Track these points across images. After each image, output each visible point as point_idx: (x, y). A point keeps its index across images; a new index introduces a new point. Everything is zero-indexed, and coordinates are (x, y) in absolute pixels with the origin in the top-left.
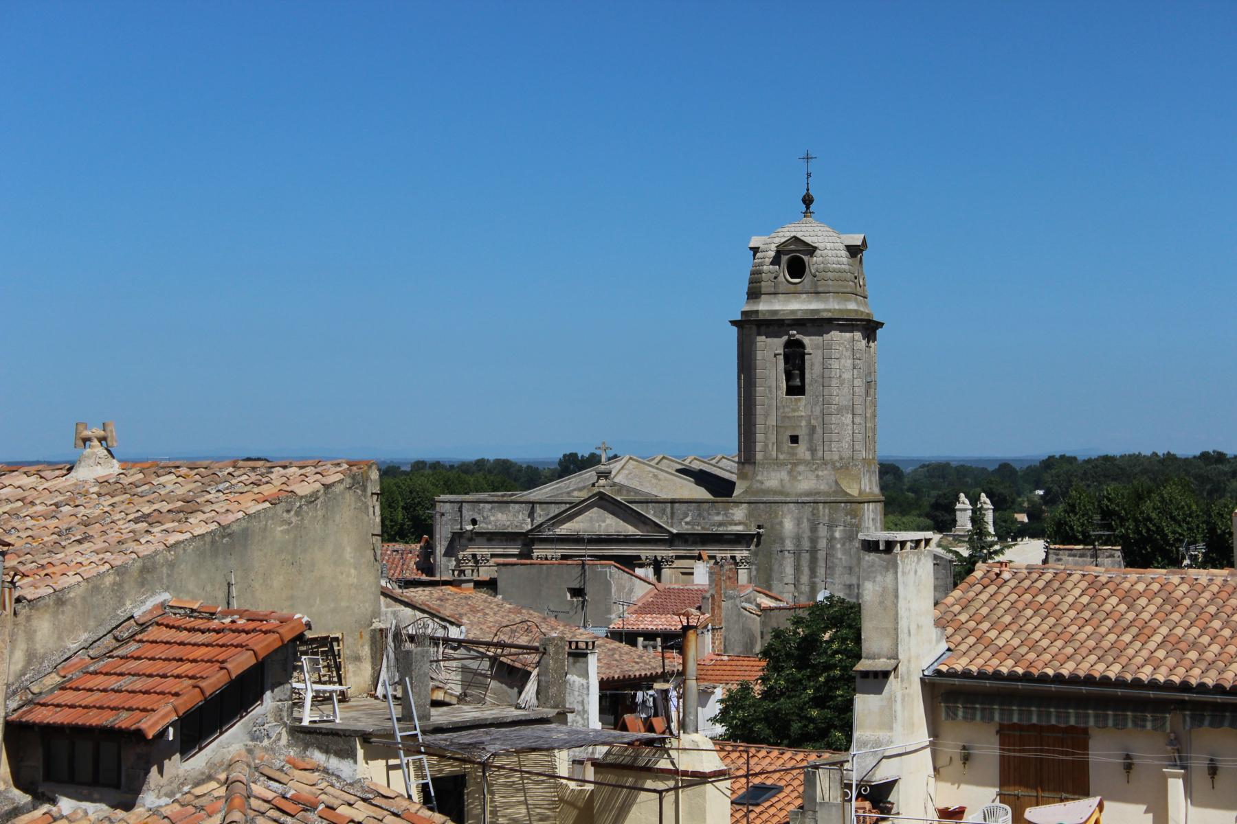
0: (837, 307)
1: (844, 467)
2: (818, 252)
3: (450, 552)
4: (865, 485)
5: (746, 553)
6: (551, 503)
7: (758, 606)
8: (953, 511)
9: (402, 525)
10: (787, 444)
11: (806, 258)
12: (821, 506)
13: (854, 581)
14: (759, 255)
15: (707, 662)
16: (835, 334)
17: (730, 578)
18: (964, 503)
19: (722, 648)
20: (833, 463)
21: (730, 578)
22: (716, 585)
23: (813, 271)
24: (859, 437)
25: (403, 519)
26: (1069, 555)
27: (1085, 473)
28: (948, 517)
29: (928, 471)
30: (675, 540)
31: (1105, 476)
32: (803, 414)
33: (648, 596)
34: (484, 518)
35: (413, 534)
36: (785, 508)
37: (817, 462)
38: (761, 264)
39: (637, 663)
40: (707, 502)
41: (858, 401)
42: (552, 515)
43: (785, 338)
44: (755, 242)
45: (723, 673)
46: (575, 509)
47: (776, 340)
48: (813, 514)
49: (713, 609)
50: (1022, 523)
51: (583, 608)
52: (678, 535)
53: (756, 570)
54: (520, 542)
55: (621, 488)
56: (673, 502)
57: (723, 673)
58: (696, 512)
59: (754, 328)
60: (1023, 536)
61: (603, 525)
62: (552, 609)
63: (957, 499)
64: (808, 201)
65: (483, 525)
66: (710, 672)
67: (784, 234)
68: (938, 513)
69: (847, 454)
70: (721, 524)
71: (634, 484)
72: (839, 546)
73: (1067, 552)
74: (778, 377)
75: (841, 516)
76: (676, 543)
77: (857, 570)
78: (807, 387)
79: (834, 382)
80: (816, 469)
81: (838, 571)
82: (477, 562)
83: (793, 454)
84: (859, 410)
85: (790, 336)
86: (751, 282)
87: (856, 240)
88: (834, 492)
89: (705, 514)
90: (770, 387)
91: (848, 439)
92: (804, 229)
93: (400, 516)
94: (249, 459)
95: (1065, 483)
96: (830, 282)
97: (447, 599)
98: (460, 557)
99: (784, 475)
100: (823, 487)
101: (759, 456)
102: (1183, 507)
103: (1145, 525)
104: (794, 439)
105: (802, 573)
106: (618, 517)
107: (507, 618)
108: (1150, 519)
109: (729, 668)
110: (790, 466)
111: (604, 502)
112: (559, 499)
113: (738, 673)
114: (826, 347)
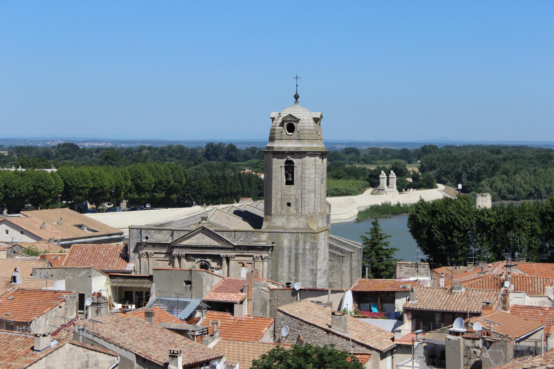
0: (308, 146)
1: (310, 217)
2: (300, 121)
3: (136, 251)
4: (320, 224)
5: (267, 255)
6: (181, 231)
7: (269, 288)
10: (286, 206)
11: (295, 124)
12: (300, 234)
13: (314, 268)
14: (274, 121)
15: (244, 319)
16: (307, 158)
17: (256, 277)
19: (252, 308)
20: (306, 216)
21: (256, 277)
22: (250, 281)
23: (298, 130)
24: (317, 203)
25: (131, 185)
26: (406, 266)
27: (438, 158)
28: (376, 181)
29: (371, 151)
30: (235, 248)
31: (447, 160)
32: (293, 193)
33: (220, 283)
34: (151, 236)
35: (135, 191)
36: (284, 235)
37: (299, 215)
38: (275, 126)
39: (202, 353)
41: (317, 187)
42: (181, 236)
43: (285, 159)
44: (274, 114)
45: (250, 325)
46: (191, 234)
47: (281, 160)
48: (297, 238)
49: (248, 291)
51: (190, 290)
52: (237, 246)
53: (271, 262)
54: (167, 247)
55: (212, 224)
56: (235, 231)
57: (250, 325)
58: (245, 236)
59: (272, 155)
60: (410, 188)
61: (204, 241)
63: (381, 173)
64: (297, 97)
65: (151, 240)
66: (245, 324)
68: (372, 179)
70: (256, 242)
72: (308, 252)
73: (405, 265)
74: (282, 177)
75: (309, 239)
76: (236, 250)
77: (315, 263)
78: (295, 181)
79: (307, 180)
81: (307, 263)
82: (148, 256)
83: (289, 211)
84: (317, 192)
85: (287, 159)
86: (271, 134)
88: (306, 228)
89: (249, 237)
90: (278, 181)
91: (313, 204)
93: (130, 184)
97: (119, 321)
98: (141, 253)
99: (284, 220)
100: (301, 226)
101: (273, 212)
103: (450, 216)
105: (292, 264)
106: (210, 237)
107: (145, 330)
108: (452, 214)
109: (253, 323)
110: (287, 216)
111: (204, 231)
112: (185, 229)
113: (257, 325)
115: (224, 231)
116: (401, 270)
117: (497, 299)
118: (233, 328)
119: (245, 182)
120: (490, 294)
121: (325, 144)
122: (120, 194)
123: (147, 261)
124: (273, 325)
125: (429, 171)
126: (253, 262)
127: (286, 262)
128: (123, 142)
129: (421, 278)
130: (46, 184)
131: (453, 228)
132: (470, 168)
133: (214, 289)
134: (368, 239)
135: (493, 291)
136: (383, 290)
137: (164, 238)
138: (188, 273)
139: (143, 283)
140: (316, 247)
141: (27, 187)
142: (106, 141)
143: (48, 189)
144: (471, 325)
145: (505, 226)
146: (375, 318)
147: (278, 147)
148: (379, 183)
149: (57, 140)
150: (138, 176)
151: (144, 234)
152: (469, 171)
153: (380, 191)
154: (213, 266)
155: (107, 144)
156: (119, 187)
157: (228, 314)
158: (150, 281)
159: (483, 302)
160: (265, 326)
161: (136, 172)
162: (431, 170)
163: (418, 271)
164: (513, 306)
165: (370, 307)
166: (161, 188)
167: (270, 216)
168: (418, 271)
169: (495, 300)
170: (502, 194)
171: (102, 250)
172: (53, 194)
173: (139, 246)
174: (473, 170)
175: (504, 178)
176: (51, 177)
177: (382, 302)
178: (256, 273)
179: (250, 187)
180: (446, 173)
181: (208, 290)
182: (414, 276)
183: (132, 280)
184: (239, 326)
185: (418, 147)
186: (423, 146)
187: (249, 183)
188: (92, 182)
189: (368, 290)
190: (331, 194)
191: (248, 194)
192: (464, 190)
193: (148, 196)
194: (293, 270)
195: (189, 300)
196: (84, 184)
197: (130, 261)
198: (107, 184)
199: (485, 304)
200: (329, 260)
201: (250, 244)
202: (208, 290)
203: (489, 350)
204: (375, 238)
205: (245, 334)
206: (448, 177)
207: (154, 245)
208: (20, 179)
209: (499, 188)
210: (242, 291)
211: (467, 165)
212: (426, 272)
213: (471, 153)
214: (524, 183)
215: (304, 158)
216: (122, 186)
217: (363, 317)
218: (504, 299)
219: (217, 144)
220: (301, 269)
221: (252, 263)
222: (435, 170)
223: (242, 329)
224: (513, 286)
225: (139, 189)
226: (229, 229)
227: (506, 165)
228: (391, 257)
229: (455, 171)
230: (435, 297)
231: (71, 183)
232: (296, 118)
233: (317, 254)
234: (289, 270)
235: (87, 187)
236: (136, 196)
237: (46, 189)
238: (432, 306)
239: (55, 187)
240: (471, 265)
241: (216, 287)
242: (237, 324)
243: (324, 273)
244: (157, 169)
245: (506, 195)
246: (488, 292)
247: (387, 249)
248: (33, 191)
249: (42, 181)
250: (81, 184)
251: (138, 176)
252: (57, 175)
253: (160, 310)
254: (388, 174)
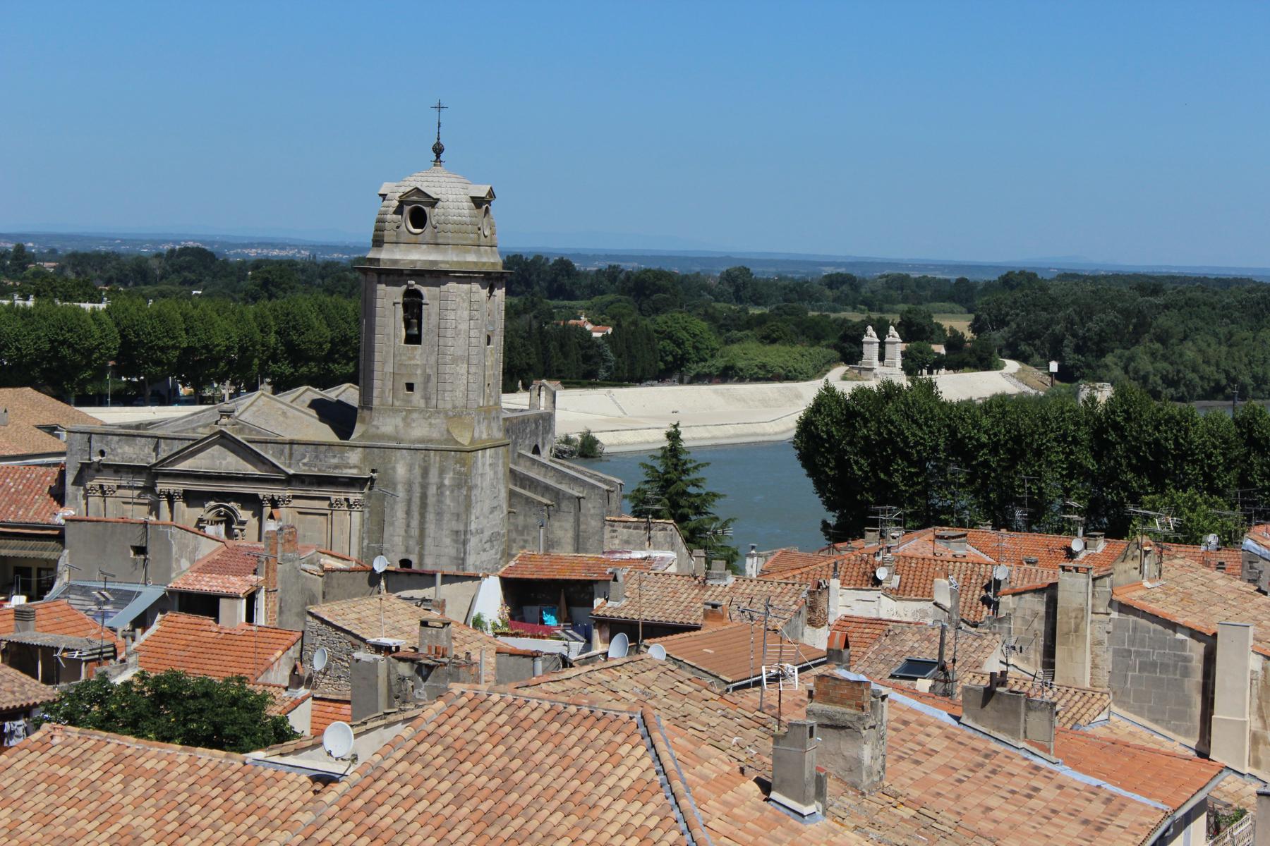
0: (455, 259)
1: (456, 416)
2: (440, 204)
3: (78, 481)
5: (359, 497)
6: (175, 439)
7: (322, 566)
8: (860, 344)
9: (275, 349)
11: (427, 209)
12: (432, 453)
13: (462, 528)
15: (237, 633)
16: (452, 286)
17: (289, 541)
19: (277, 608)
20: (446, 413)
22: (271, 550)
24: (473, 386)
26: (624, 527)
29: (887, 282)
30: (290, 480)
31: (1035, 305)
32: (419, 362)
36: (398, 453)
37: (431, 410)
38: (385, 213)
40: (331, 445)
41: (474, 351)
42: (175, 450)
43: (404, 287)
46: (197, 447)
47: (395, 289)
48: (425, 461)
49: (267, 573)
50: (939, 354)
52: (295, 476)
54: (145, 475)
55: (243, 428)
56: (292, 443)
58: (314, 454)
59: (375, 276)
60: (939, 368)
61: (224, 462)
62: (104, 570)
63: (865, 331)
64: (438, 150)
65: (111, 457)
66: (238, 643)
68: (846, 345)
69: (460, 402)
70: (336, 467)
71: (260, 422)
72: (448, 493)
74: (397, 326)
76: (294, 483)
78: (423, 336)
79: (449, 333)
80: (429, 417)
81: (447, 517)
82: (103, 492)
83: (410, 402)
84: (474, 360)
85: (409, 286)
86: (376, 230)
87: (482, 191)
88: (446, 440)
89: (322, 456)
90: (388, 335)
91: (462, 388)
92: (430, 179)
95: (994, 312)
96: (449, 234)
98: (88, 487)
99: (398, 421)
100: (435, 435)
101: (376, 402)
102: (926, 410)
103: (886, 427)
106: (238, 455)
108: (892, 422)
110: (404, 413)
111: (224, 440)
112: (184, 435)
114: (442, 299)
115: (266, 442)
116: (615, 534)
117: (795, 603)
118: (210, 651)
119: (553, 346)
120: (785, 591)
121: (501, 254)
122: (249, 366)
123: (102, 505)
124: (298, 646)
125: (993, 330)
126: (329, 512)
127: (400, 513)
128: (334, 248)
129: (657, 554)
130: (78, 336)
131: (894, 454)
132: (1083, 324)
133: (200, 565)
134: (657, 471)
135: (793, 585)
136: (567, 578)
137: (138, 453)
138: (140, 529)
139: (44, 549)
140: (466, 481)
141: (35, 344)
142: (295, 246)
143: (84, 348)
144: (644, 649)
145: (1009, 451)
146: (539, 637)
147: (389, 260)
148: (862, 353)
149: (186, 241)
150: (291, 324)
151: (97, 445)
152: (1081, 332)
153: (863, 372)
154: (243, 519)
155: (299, 252)
156: (247, 347)
157: (209, 621)
158: (59, 546)
159: (706, 604)
160: (276, 646)
161: (288, 315)
162: (998, 329)
163: (649, 538)
164: (843, 618)
165: (541, 613)
166: (346, 352)
167: (368, 412)
168: (649, 538)
169: (791, 603)
170: (1150, 387)
171: (12, 478)
172: (95, 361)
173: (85, 471)
174: (1089, 330)
175: (1157, 350)
176: (92, 322)
177: (569, 604)
178: (290, 533)
179: (566, 355)
180: (1030, 337)
181: (184, 568)
182: (642, 550)
183: (40, 544)
184: (225, 647)
185: (994, 277)
186: (1005, 273)
187: (562, 346)
188: (185, 336)
189: (534, 577)
190: (751, 376)
191: (559, 371)
192: (1063, 376)
193: (315, 370)
194: (415, 532)
195: (136, 588)
196: (165, 340)
197: (67, 503)
198: (220, 341)
199: (710, 607)
200: (509, 512)
201: (324, 471)
202: (184, 568)
203: (427, 683)
204: (671, 470)
205: (233, 664)
206: (1034, 346)
207: (118, 469)
208: (19, 324)
209: (1142, 373)
210: (255, 572)
211: (1077, 319)
212: (669, 539)
213: (1093, 292)
214: (1204, 362)
215: (444, 284)
216: (254, 346)
217: (513, 635)
218: (811, 602)
219: (531, 258)
220: (431, 528)
221: (326, 515)
222: (1006, 328)
223: (229, 653)
224: (897, 578)
225: (296, 355)
226: (280, 438)
227: (1164, 321)
228: (706, 513)
229: (1050, 331)
230: (665, 594)
231: (138, 336)
232: (429, 196)
233: (468, 497)
234: (406, 531)
235: (174, 347)
236: (288, 370)
237: (78, 347)
238: (652, 614)
239: (99, 344)
240: (873, 534)
241: (205, 562)
242: (221, 641)
243: (490, 541)
244: (336, 307)
245: (1159, 388)
246: (783, 585)
247: (698, 495)
248: (49, 352)
249: (70, 331)
250: (159, 339)
251: (291, 324)
252: (105, 317)
253: (66, 607)
254: (882, 332)
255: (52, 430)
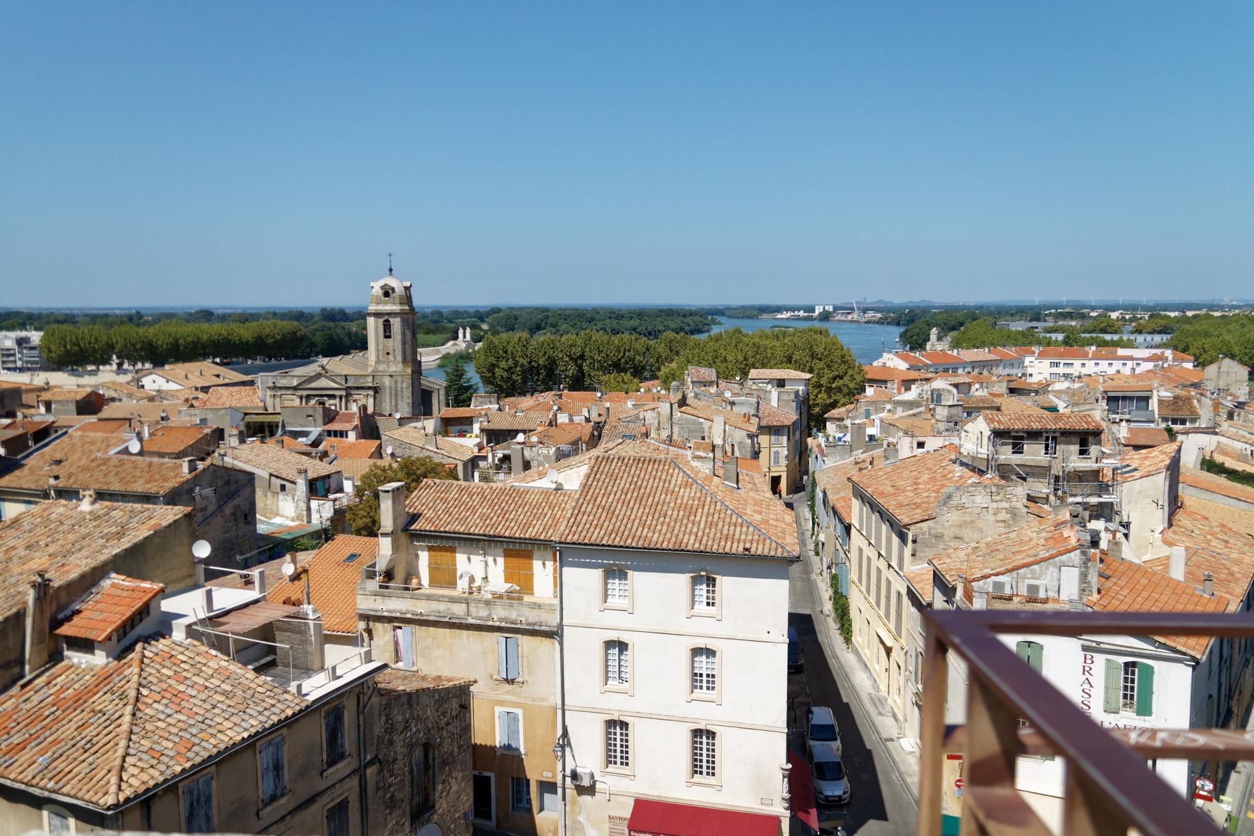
18: (461, 331)
64: (391, 270)
67: (382, 283)
87: (408, 284)
94: (898, 573)
99: (385, 366)
104: (388, 354)
194: (393, 404)
220: (400, 403)
255: (218, 376)
